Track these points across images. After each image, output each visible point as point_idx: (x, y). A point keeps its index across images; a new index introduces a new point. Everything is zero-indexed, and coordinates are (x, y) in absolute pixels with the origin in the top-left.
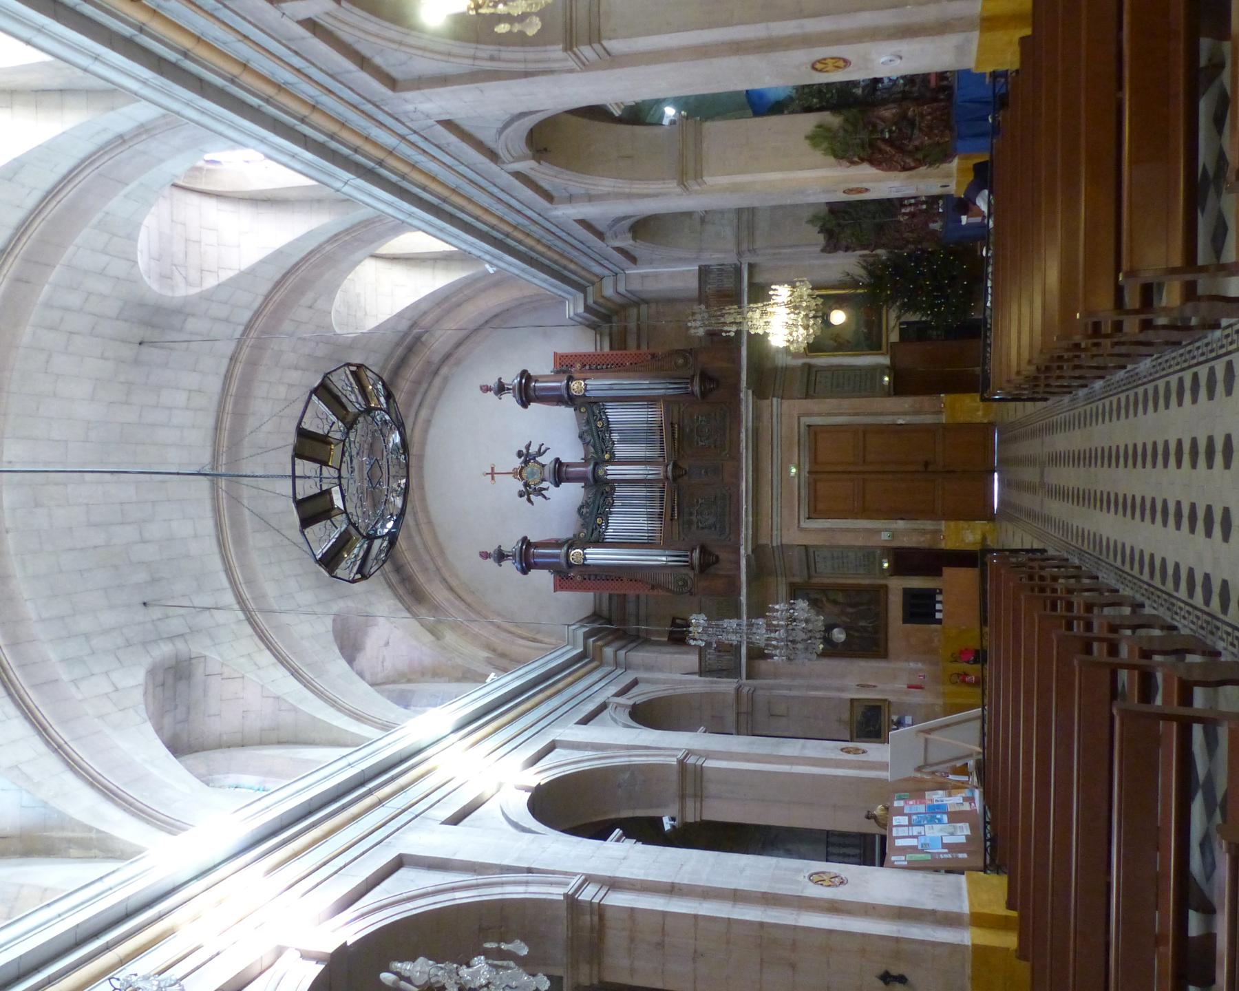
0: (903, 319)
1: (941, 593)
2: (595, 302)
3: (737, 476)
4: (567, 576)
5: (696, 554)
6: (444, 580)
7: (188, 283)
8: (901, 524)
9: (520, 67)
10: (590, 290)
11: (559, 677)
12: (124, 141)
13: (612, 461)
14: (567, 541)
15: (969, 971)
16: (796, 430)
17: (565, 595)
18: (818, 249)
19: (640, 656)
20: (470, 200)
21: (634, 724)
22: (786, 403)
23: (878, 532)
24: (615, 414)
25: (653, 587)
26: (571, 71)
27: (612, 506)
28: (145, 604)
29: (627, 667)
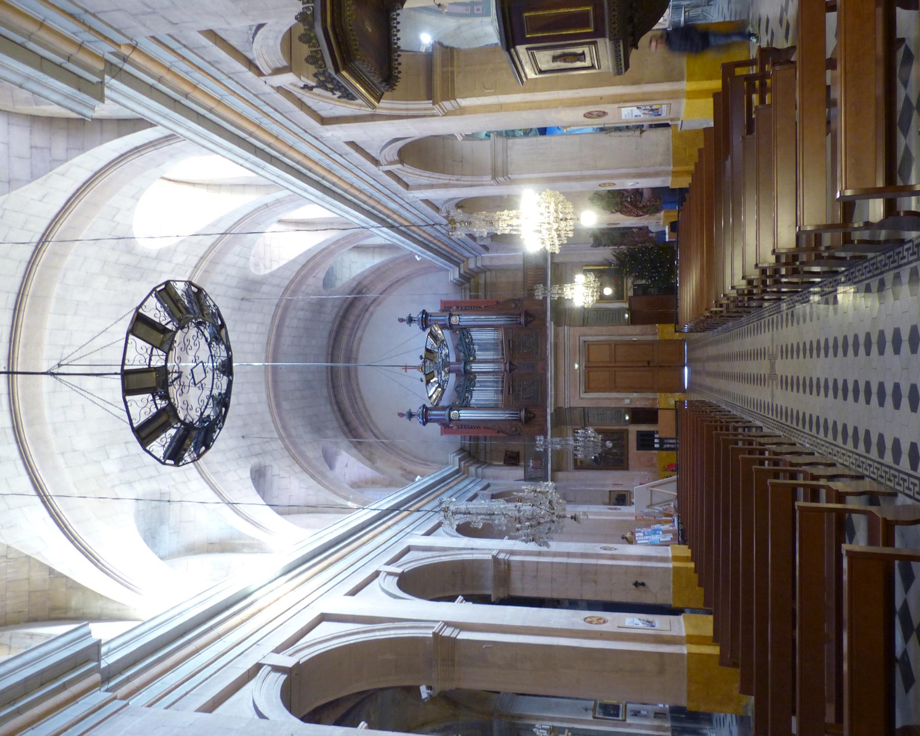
0: (635, 283)
1: (657, 433)
2: (464, 272)
3: (545, 369)
4: (447, 426)
5: (523, 413)
6: (371, 431)
7: (265, 268)
8: (635, 395)
10: (462, 265)
11: (449, 480)
12: (268, 207)
13: (474, 361)
14: (447, 407)
15: (671, 578)
16: (578, 345)
17: (445, 437)
18: (590, 245)
19: (489, 471)
20: (386, 207)
21: (459, 535)
22: (572, 329)
23: (623, 399)
24: (476, 335)
25: (498, 432)
26: (492, 185)
27: (474, 386)
28: (243, 437)
29: (483, 477)
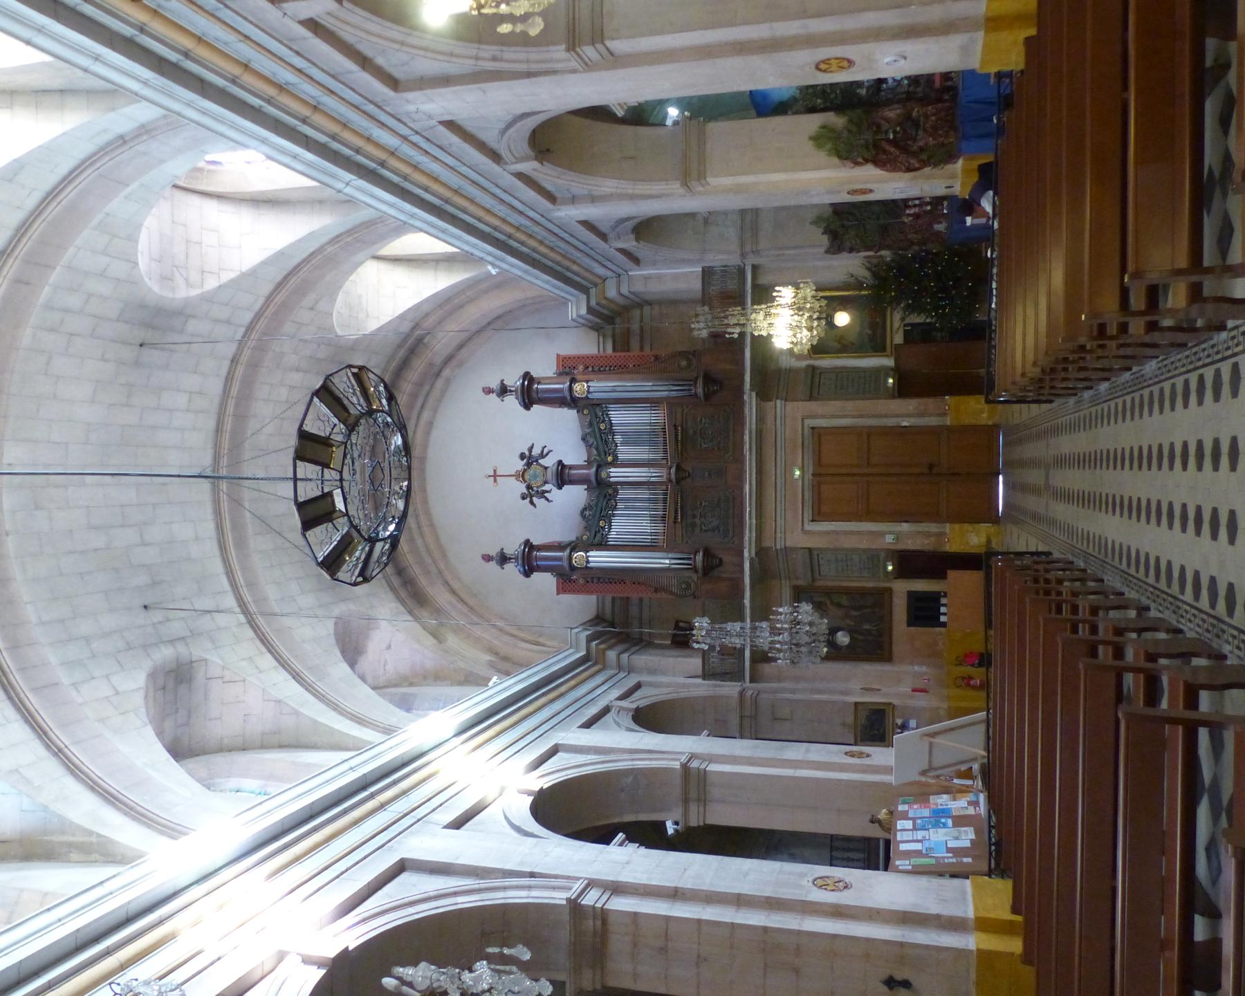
0: (908, 321)
1: (945, 596)
2: (597, 304)
3: (740, 478)
4: (570, 579)
5: (699, 557)
6: (446, 583)
7: (189, 284)
8: (905, 527)
9: (523, 67)
10: (593, 291)
11: (562, 680)
12: (125, 142)
13: (615, 463)
14: (570, 544)
15: (973, 976)
16: (800, 432)
17: (568, 598)
18: (822, 250)
19: (643, 659)
21: (637, 728)
22: (790, 405)
23: (882, 534)
24: (618, 416)
25: (656, 590)
26: (574, 71)
27: (615, 508)
28: (145, 607)
29: (630, 670)
